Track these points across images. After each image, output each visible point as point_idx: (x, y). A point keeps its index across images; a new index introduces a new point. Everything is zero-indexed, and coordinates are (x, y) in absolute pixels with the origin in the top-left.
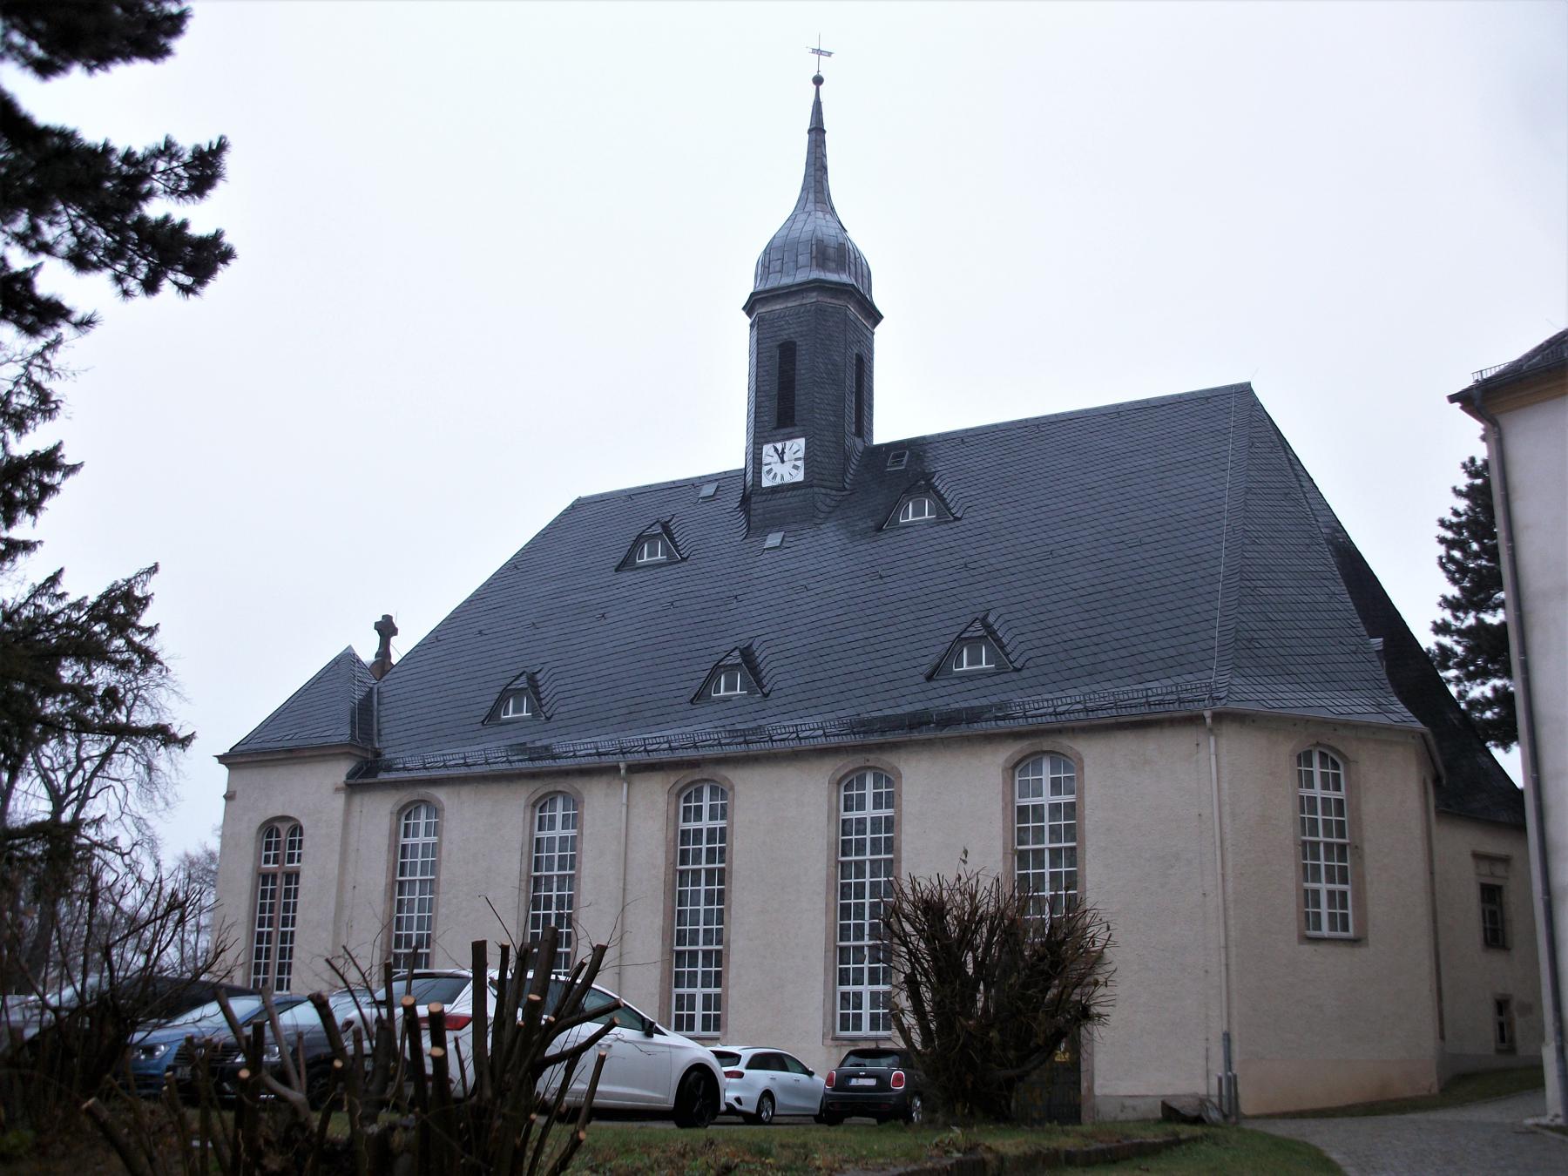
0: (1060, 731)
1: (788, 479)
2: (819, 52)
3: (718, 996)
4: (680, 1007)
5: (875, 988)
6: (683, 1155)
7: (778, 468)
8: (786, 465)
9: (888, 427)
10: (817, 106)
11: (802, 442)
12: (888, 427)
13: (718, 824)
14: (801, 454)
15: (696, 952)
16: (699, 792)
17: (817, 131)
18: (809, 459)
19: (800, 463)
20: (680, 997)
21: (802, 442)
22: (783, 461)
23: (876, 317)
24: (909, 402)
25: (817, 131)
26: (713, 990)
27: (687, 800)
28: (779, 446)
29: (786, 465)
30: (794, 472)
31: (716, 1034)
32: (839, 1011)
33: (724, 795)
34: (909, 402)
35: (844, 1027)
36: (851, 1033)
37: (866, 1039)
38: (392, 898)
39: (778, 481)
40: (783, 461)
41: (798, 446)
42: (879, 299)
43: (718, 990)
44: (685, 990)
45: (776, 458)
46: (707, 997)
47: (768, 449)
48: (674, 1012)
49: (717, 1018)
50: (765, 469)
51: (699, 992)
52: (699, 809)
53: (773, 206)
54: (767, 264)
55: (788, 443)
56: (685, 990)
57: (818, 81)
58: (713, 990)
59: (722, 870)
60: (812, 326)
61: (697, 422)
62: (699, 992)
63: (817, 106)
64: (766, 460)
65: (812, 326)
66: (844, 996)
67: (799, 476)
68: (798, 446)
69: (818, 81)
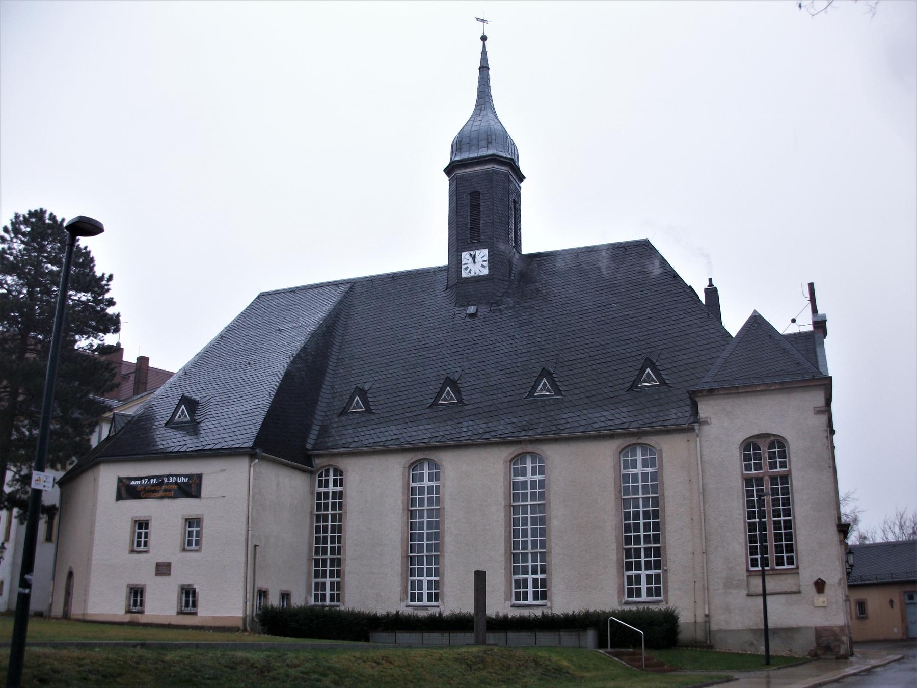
0: (435, 448)
1: (478, 273)
2: (484, 21)
3: (338, 583)
4: (517, 586)
5: (332, 580)
6: (138, 663)
7: (471, 266)
8: (476, 264)
9: (529, 246)
10: (484, 53)
11: (486, 251)
12: (529, 246)
13: (338, 489)
14: (486, 258)
15: (640, 549)
16: (327, 471)
17: (484, 68)
18: (491, 261)
19: (486, 264)
20: (317, 584)
21: (486, 251)
22: (474, 262)
23: (521, 178)
24: (540, 233)
25: (484, 68)
26: (336, 580)
27: (321, 476)
28: (472, 253)
29: (476, 264)
30: (482, 269)
31: (544, 602)
32: (626, 587)
33: (342, 474)
34: (540, 233)
35: (517, 599)
36: (635, 599)
37: (425, 607)
38: (134, 532)
39: (472, 274)
40: (474, 262)
41: (483, 254)
42: (523, 170)
43: (338, 580)
44: (416, 579)
45: (471, 260)
46: (332, 584)
47: (465, 255)
48: (410, 591)
49: (338, 595)
50: (464, 267)
51: (425, 579)
52: (327, 481)
53: (459, 113)
54: (458, 145)
55: (478, 252)
56: (416, 579)
57: (484, 38)
58: (336, 580)
59: (340, 515)
60: (484, 184)
61: (418, 237)
62: (425, 579)
63: (484, 53)
64: (464, 261)
65: (484, 184)
66: (517, 581)
67: (486, 272)
68: (483, 254)
69: (484, 38)
